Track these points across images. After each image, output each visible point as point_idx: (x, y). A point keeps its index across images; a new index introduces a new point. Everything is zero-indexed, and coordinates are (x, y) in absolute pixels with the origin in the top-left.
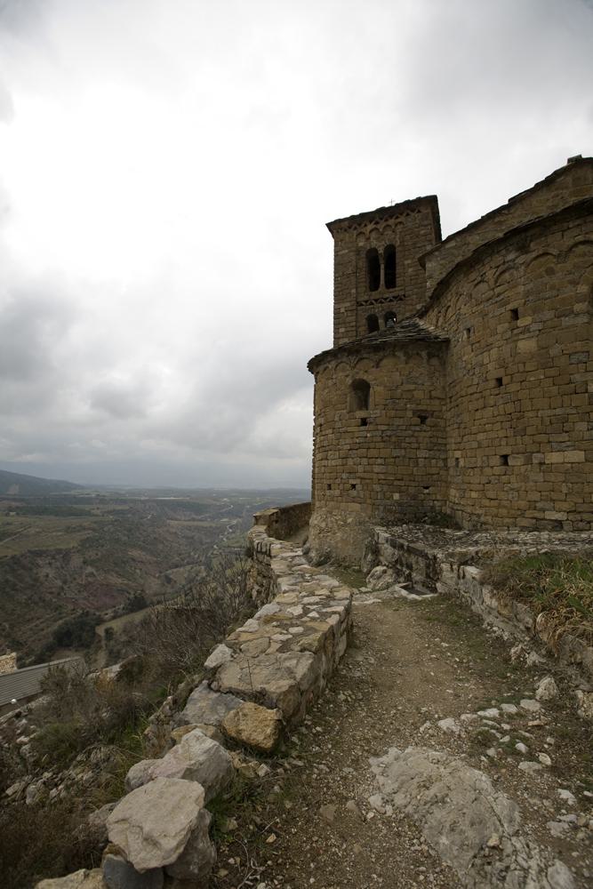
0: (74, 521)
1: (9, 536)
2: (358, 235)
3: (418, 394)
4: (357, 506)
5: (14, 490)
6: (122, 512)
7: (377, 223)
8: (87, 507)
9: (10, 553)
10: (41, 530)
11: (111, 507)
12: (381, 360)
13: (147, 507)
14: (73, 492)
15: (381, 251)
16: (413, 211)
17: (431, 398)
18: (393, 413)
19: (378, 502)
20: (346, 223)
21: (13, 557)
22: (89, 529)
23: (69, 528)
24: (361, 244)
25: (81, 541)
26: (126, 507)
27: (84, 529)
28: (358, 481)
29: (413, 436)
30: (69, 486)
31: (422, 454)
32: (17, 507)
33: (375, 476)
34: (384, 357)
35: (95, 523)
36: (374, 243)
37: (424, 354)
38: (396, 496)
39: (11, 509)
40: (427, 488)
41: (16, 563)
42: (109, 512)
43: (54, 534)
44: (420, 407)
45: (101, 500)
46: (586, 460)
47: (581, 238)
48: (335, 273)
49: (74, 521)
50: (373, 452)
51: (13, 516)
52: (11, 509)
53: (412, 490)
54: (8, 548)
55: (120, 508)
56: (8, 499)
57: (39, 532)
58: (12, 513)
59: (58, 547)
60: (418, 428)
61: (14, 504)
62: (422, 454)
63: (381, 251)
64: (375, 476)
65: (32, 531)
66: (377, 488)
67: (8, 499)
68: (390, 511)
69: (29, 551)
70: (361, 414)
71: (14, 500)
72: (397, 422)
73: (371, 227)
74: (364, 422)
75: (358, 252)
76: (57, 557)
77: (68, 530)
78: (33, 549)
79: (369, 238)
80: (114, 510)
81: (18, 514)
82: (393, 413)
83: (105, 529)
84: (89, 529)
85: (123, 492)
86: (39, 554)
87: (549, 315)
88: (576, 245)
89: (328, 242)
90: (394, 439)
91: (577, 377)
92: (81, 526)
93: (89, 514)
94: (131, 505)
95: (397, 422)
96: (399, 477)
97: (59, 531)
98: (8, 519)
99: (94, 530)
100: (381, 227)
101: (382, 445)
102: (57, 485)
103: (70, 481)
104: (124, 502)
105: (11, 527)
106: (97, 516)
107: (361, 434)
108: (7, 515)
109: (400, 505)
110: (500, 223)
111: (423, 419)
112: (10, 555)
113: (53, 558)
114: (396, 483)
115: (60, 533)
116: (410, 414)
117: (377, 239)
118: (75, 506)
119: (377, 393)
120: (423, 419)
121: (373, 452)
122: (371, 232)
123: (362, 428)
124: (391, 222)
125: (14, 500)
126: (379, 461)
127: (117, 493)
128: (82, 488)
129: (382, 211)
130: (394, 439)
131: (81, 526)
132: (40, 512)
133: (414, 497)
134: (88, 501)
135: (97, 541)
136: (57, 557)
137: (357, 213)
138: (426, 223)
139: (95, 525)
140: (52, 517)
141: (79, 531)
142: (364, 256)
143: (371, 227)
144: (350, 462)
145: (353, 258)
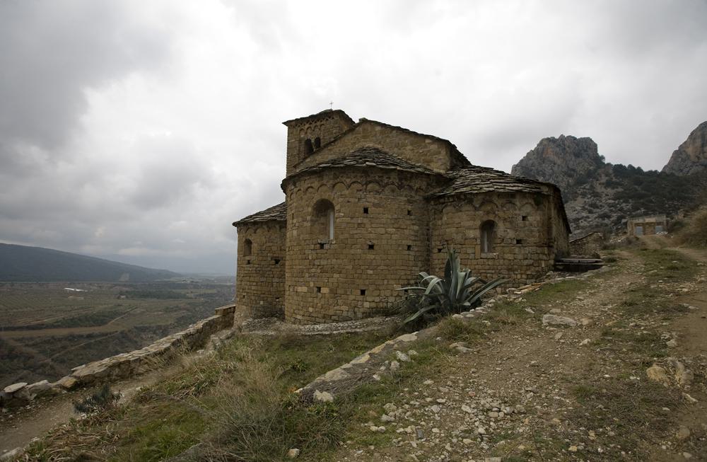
0: (171, 303)
1: (120, 315)
2: (301, 130)
3: (274, 248)
4: (244, 307)
5: (125, 278)
6: (211, 295)
7: (311, 124)
8: (183, 292)
9: (120, 329)
10: (145, 310)
11: (202, 291)
12: (256, 230)
13: (232, 290)
14: (172, 280)
15: (313, 141)
16: (330, 118)
17: (281, 250)
18: (261, 258)
19: (253, 305)
20: (294, 122)
21: (122, 333)
22: (184, 309)
23: (167, 308)
24: (302, 136)
25: (177, 319)
26: (214, 291)
27: (180, 309)
28: (245, 294)
29: (270, 271)
30: (169, 275)
31: (276, 280)
32: (127, 292)
33: (252, 291)
34: (258, 228)
35: (189, 304)
36: (309, 136)
37: (277, 227)
38: (262, 303)
39: (122, 294)
40: (278, 298)
41: (123, 337)
42: (201, 295)
43: (156, 313)
44: (275, 255)
45: (195, 285)
46: (308, 292)
47: (309, 185)
48: (288, 153)
49: (171, 303)
50: (252, 279)
51: (123, 299)
52: (122, 294)
53: (269, 300)
54: (118, 325)
55: (210, 291)
56: (119, 285)
57: (144, 312)
58: (122, 297)
59: (159, 324)
60: (273, 266)
61: (125, 289)
62: (276, 280)
63: (313, 141)
64: (252, 291)
65: (138, 311)
66: (253, 298)
67: (119, 285)
68: (258, 310)
69: (136, 328)
70: (247, 258)
71: (125, 286)
72: (263, 263)
73: (307, 126)
74: (249, 262)
75: (300, 141)
76: (157, 332)
77: (167, 310)
78: (138, 326)
79: (306, 133)
80: (205, 294)
81: (127, 297)
82: (261, 258)
83: (197, 309)
84: (184, 309)
85: (213, 279)
86: (143, 329)
87: (300, 219)
88: (309, 188)
89: (286, 128)
90: (261, 272)
91: (307, 252)
92: (177, 307)
93: (184, 297)
94: (219, 289)
95: (263, 263)
96: (263, 292)
97: (160, 311)
98: (119, 302)
99: (188, 310)
100: (314, 125)
101: (255, 275)
102: (160, 273)
103: (170, 270)
104: (213, 287)
105: (122, 308)
106: (191, 298)
107: (248, 269)
108: (119, 298)
109: (263, 307)
110: (330, 150)
111: (277, 262)
112: (119, 331)
113: (154, 333)
114: (262, 296)
115: (160, 313)
116: (269, 259)
117: (310, 133)
118: (174, 290)
119: (255, 246)
120: (277, 262)
121: (252, 279)
122: (308, 129)
123: (248, 265)
124: (318, 123)
125: (125, 286)
126: (254, 284)
127: (207, 280)
128: (180, 275)
129: (312, 117)
130: (261, 272)
131: (177, 307)
132: (145, 296)
133: (271, 304)
134: (185, 286)
135: (190, 318)
136: (157, 332)
137: (299, 118)
138: (336, 125)
139: (188, 306)
140: (155, 300)
141: (176, 311)
142: (303, 143)
143: (307, 126)
144: (243, 283)
145: (298, 145)
